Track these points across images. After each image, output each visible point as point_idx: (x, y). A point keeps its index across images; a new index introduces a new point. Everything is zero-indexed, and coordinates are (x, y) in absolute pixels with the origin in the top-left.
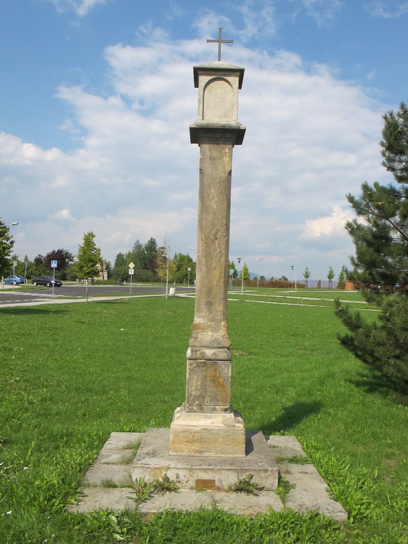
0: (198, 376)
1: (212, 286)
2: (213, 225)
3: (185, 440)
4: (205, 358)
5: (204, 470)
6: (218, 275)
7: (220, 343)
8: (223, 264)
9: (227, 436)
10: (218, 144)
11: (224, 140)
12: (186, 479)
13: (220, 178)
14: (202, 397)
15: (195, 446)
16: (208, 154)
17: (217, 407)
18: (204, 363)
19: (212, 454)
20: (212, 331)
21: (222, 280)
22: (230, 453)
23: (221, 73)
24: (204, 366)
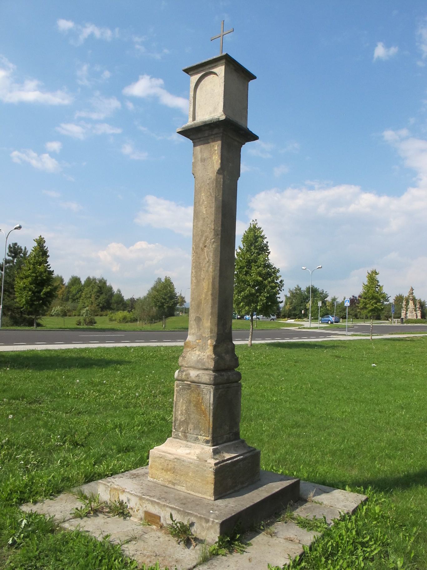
0: (183, 400)
1: (201, 300)
2: (203, 232)
3: (161, 467)
4: (189, 380)
5: (153, 502)
6: (206, 288)
7: (203, 364)
8: (211, 274)
9: (197, 471)
10: (209, 143)
11: (213, 137)
12: (137, 508)
13: (209, 179)
14: (186, 422)
15: (169, 476)
16: (199, 156)
17: (199, 436)
18: (189, 385)
19: (184, 489)
20: (199, 350)
21: (210, 292)
22: (199, 492)
23: (207, 67)
24: (188, 389)
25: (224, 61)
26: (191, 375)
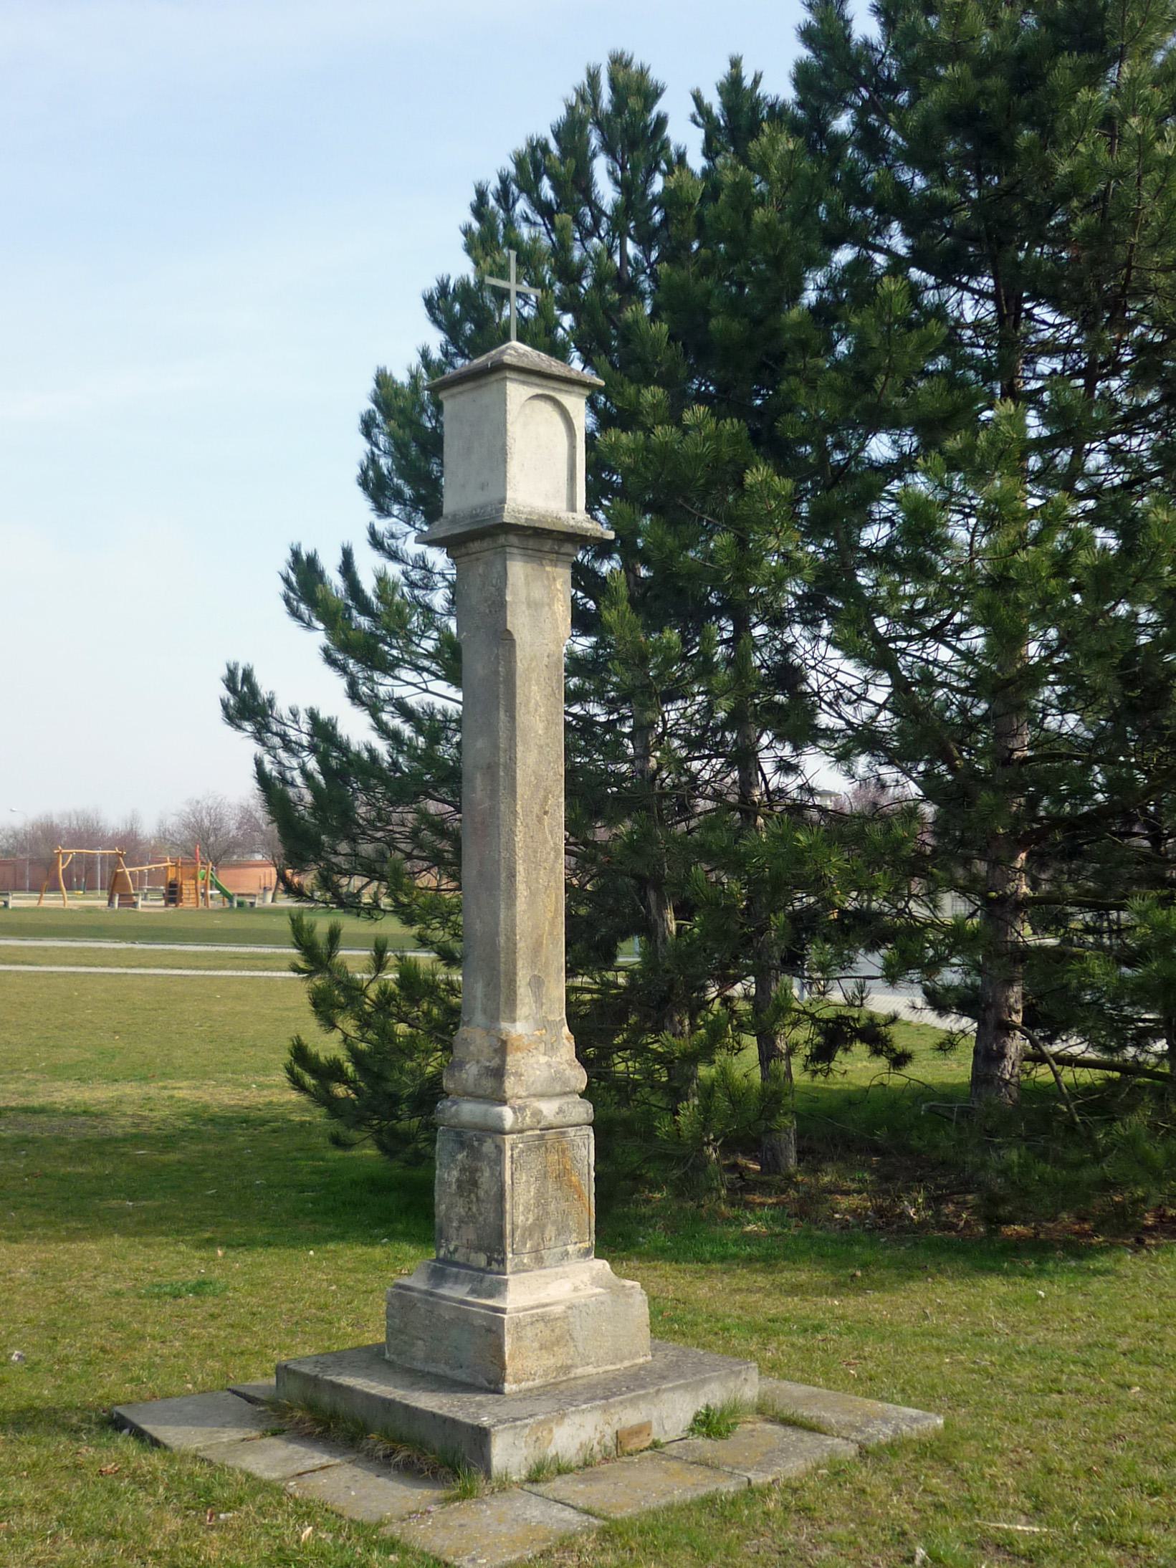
14: (539, 1225)
18: (541, 1137)
19: (590, 1370)
25: (587, 393)
26: (545, 1112)
